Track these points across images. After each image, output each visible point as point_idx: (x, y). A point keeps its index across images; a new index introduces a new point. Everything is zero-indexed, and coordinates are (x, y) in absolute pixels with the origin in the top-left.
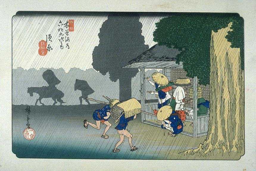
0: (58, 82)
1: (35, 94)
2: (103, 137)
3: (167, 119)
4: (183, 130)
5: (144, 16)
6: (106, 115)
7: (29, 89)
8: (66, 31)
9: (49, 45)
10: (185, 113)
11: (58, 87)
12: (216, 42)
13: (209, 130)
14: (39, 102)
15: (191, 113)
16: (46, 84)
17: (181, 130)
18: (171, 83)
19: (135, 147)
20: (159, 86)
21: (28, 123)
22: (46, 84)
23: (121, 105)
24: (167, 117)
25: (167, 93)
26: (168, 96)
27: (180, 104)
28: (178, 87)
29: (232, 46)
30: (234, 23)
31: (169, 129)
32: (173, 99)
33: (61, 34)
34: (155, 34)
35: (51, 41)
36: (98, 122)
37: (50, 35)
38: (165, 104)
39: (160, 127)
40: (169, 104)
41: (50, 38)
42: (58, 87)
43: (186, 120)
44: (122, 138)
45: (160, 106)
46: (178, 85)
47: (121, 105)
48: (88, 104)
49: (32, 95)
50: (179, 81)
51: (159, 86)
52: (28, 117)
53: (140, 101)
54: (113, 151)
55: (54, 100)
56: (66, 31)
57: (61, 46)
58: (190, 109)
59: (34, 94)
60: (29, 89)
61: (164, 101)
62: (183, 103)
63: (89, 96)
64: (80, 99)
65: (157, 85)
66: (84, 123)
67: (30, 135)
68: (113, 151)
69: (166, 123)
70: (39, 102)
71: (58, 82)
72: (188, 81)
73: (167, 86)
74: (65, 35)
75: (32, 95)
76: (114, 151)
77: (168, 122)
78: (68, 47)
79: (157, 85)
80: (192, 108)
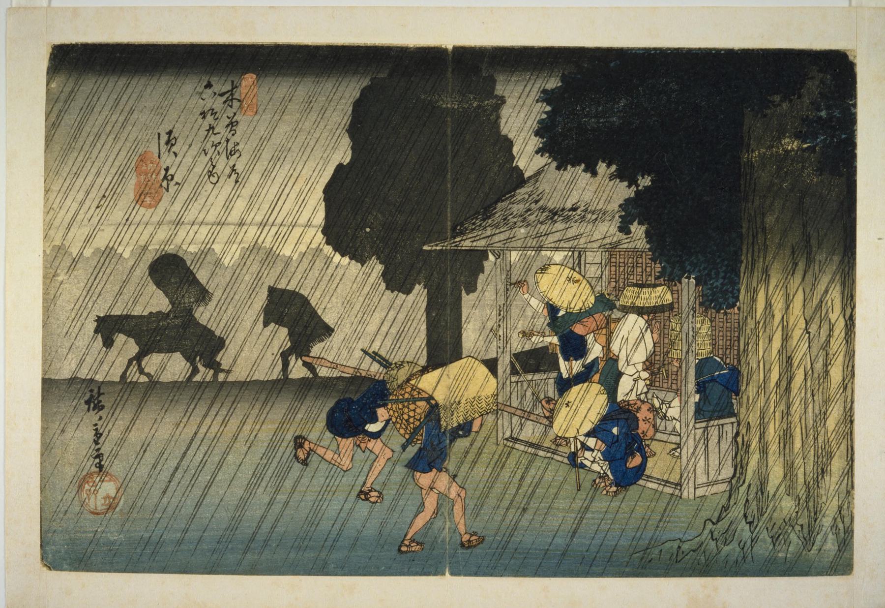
1: (120, 339)
2: (363, 497)
4: (647, 472)
5: (534, 69)
6: (374, 419)
7: (100, 320)
9: (167, 169)
10: (653, 409)
11: (204, 315)
13: (740, 467)
17: (640, 470)
18: (604, 303)
20: (561, 313)
23: (427, 382)
24: (587, 427)
25: (590, 338)
26: (595, 351)
27: (635, 376)
29: (483, 273)
30: (546, 141)
31: (595, 467)
32: (612, 361)
33: (211, 128)
35: (176, 154)
36: (347, 443)
37: (170, 133)
38: (583, 377)
39: (566, 460)
40: (596, 377)
43: (659, 436)
44: (431, 503)
45: (564, 385)
46: (627, 310)
48: (311, 376)
49: (108, 343)
50: (629, 296)
51: (561, 313)
52: (96, 430)
53: (492, 365)
54: (399, 550)
55: (190, 359)
59: (120, 339)
60: (100, 320)
61: (577, 366)
62: (645, 375)
63: (316, 349)
64: (285, 357)
65: (552, 309)
66: (296, 449)
68: (399, 550)
69: (585, 447)
70: (134, 368)
72: (659, 295)
73: (588, 313)
75: (108, 343)
76: (404, 549)
77: (591, 442)
78: (234, 176)
79: (552, 309)
80: (678, 392)
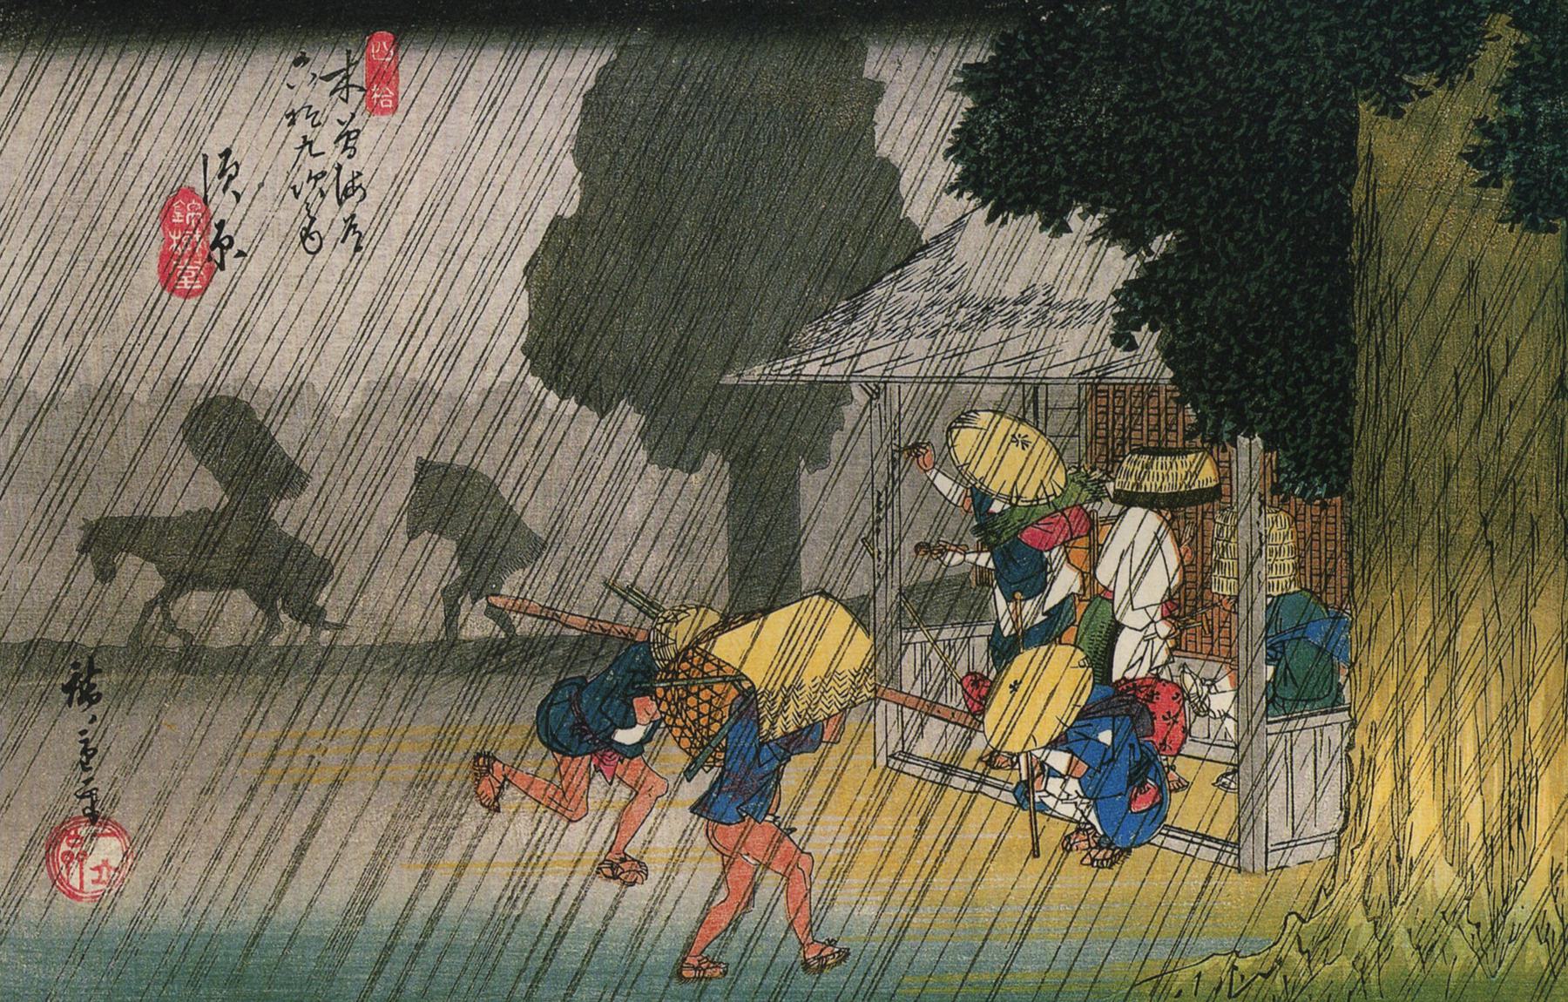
0: (290, 478)
3: (1053, 745)
8: (341, 123)
11: (288, 514)
12: (505, 342)
14: (155, 618)
15: (1221, 701)
16: (207, 493)
19: (831, 943)
21: (87, 782)
22: (207, 493)
23: (728, 647)
26: (1065, 582)
28: (1498, 15)
32: (1096, 595)
34: (964, 144)
38: (1049, 631)
40: (1069, 635)
41: (231, 178)
42: (288, 514)
45: (1004, 650)
47: (728, 647)
51: (997, 507)
56: (341, 123)
57: (306, 234)
58: (1211, 669)
59: (130, 564)
65: (980, 498)
67: (98, 868)
71: (290, 478)
74: (334, 155)
75: (106, 574)
78: (352, 239)
80: (1231, 661)
